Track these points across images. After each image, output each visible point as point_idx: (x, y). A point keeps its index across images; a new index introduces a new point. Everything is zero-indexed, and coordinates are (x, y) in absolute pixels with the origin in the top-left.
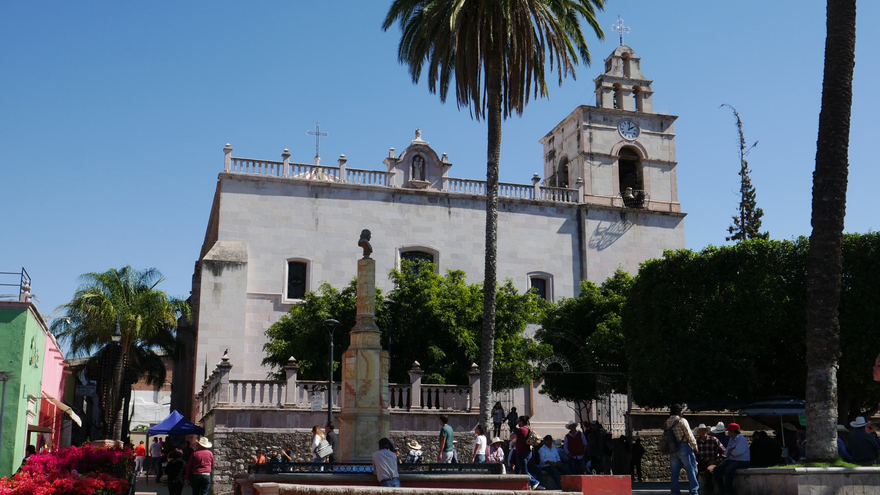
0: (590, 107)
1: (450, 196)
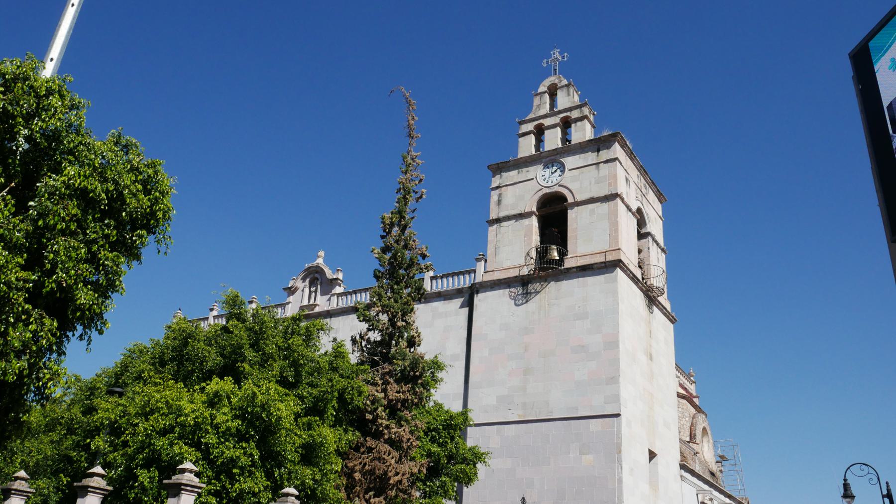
0: (498, 164)
1: (331, 312)
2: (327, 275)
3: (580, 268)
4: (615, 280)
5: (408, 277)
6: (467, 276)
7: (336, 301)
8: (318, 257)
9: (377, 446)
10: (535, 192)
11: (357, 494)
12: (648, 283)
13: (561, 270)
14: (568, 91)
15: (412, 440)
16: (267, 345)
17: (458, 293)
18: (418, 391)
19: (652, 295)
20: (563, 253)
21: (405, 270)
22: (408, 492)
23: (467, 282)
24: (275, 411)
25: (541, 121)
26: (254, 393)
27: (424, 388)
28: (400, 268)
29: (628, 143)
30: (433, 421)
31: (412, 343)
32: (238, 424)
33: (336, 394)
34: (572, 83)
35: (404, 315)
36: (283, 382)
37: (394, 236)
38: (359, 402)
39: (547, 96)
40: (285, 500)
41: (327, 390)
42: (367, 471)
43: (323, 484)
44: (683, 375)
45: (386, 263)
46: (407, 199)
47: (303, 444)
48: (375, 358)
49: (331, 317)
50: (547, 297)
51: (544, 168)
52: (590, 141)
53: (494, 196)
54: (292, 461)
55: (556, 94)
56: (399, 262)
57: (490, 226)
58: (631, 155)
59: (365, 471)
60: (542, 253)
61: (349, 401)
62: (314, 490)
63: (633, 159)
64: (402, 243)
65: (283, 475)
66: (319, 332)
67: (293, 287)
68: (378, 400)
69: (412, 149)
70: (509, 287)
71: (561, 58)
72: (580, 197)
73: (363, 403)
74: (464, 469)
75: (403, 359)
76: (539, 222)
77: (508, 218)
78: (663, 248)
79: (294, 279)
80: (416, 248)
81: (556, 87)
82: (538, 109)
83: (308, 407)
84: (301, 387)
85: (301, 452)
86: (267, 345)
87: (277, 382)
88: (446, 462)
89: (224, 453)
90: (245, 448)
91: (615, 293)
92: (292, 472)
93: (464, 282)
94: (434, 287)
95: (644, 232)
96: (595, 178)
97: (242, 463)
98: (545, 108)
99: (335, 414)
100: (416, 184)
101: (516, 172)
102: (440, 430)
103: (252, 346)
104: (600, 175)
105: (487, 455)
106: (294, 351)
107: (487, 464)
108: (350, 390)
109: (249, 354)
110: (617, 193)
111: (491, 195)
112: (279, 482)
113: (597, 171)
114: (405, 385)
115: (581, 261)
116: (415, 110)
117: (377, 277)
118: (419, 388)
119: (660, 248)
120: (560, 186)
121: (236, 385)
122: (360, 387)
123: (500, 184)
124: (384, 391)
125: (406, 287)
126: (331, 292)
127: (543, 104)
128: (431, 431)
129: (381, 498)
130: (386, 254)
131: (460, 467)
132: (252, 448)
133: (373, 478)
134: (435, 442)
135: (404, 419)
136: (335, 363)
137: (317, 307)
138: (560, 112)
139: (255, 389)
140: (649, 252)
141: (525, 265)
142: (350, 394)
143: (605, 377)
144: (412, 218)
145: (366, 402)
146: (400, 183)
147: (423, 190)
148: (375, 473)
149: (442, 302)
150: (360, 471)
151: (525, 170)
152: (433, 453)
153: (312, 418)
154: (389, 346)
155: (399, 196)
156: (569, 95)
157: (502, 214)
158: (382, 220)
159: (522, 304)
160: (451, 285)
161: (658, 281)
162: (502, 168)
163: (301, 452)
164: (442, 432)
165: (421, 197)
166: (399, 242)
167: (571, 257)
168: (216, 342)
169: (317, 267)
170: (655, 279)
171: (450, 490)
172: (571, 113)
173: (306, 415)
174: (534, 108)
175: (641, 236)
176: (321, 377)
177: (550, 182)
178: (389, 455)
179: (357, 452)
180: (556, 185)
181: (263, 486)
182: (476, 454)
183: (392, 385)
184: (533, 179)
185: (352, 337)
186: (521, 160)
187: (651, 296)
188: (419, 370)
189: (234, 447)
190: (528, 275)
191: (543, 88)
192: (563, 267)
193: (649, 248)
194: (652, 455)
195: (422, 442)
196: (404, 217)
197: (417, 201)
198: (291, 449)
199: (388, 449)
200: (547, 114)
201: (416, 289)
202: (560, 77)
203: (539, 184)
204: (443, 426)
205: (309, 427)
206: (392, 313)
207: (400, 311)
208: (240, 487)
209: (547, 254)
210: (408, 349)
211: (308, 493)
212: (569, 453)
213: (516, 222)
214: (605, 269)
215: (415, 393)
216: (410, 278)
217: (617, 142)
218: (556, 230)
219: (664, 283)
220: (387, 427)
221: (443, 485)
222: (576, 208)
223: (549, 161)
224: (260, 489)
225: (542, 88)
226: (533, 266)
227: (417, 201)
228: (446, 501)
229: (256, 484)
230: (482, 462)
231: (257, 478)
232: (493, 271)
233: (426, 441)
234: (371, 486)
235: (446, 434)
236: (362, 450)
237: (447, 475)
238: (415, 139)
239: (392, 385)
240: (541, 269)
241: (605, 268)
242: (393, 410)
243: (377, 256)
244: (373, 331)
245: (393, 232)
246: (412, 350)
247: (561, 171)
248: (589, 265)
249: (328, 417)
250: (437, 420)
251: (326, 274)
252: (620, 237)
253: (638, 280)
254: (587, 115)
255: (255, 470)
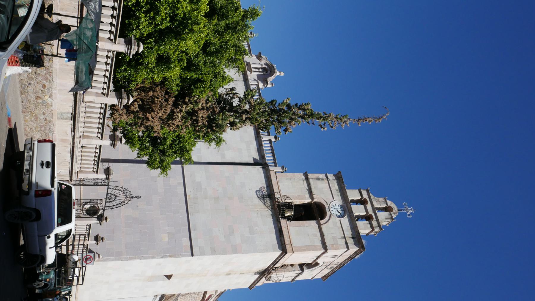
0: (342, 177)
2: (270, 78)
3: (280, 229)
4: (274, 251)
5: (273, 121)
6: (273, 161)
7: (254, 84)
8: (280, 72)
9: (169, 104)
10: (326, 200)
11: (140, 93)
12: (273, 271)
13: (279, 217)
14: (389, 218)
15: (173, 126)
16: (228, 34)
17: (262, 156)
18: (204, 129)
19: (266, 274)
20: (289, 218)
21: (277, 119)
22: (142, 125)
23: (269, 162)
24: (190, 37)
25: (369, 203)
26: (199, 24)
27: (205, 134)
28: (277, 116)
29: (358, 256)
30: (185, 140)
31: (233, 125)
32: (180, 15)
33: (200, 77)
34: (393, 221)
35: (250, 119)
36: (207, 45)
37: (297, 112)
38: (196, 92)
39: (385, 206)
40: (135, 45)
41: (203, 71)
42: (154, 99)
43: (145, 69)
44: (217, 297)
45: (280, 107)
46: (320, 119)
47: (169, 56)
48: (223, 102)
49: (244, 81)
50: (262, 209)
51: (340, 205)
52: (359, 233)
53: (322, 176)
54: (159, 50)
55: (386, 211)
56: (282, 115)
57: (303, 174)
58: (351, 258)
59: (154, 98)
60: (289, 206)
61: (196, 86)
62: (141, 64)
63: (348, 260)
64: (293, 117)
65: (151, 44)
66: (237, 68)
67: (261, 58)
68: (197, 105)
69: (351, 121)
70: (267, 187)
71: (408, 213)
72: (324, 227)
73: (195, 95)
74: (156, 161)
75: (222, 119)
76: (307, 203)
77: (309, 185)
78: (294, 280)
79: (266, 59)
80: (290, 125)
81: (391, 211)
82: (376, 200)
83: (192, 60)
84: (204, 56)
85: (165, 55)
86: (228, 34)
87: (206, 41)
88: (161, 149)
89: (163, 7)
90: (166, 20)
91: (266, 250)
92: (152, 50)
93: (269, 160)
94: (265, 142)
95: (304, 268)
96: (336, 236)
97: (157, 18)
98: (378, 205)
99: (188, 77)
100: (330, 124)
101: (337, 188)
102: (180, 145)
103: (227, 25)
104: (338, 239)
105: (166, 174)
106: (225, 52)
107: (160, 175)
108: (203, 86)
109: (223, 23)
110: (327, 250)
111: (322, 174)
112: (146, 42)
113: (340, 237)
114: (207, 121)
115: (285, 229)
116: (375, 122)
117: (272, 102)
118: (205, 130)
119: (295, 278)
120: (330, 215)
121: (204, 14)
122: (205, 92)
123: (330, 179)
124: (203, 109)
125: (266, 120)
126: (259, 81)
127: (380, 203)
128: (179, 139)
129: (138, 109)
130: (286, 107)
131: (158, 158)
132: (166, 24)
133: (150, 103)
134: (172, 142)
135: (186, 121)
136: (219, 77)
137: (250, 73)
138: (375, 214)
139: (202, 25)
140: (292, 271)
141: (281, 196)
142: (201, 86)
143: (215, 246)
144: (308, 123)
145: (196, 97)
146: (330, 114)
147: (326, 129)
148: (153, 104)
149: (256, 147)
150: (153, 95)
151: (339, 194)
152: (166, 141)
153: (186, 61)
154: (230, 111)
155: (322, 114)
156: (386, 219)
157: (311, 181)
158: (307, 103)
159: (257, 195)
160: (267, 152)
161: (275, 277)
162: (339, 180)
163: (165, 55)
164: (178, 146)
165: (322, 127)
166: (294, 115)
167: (287, 223)
168: (230, 3)
169: (274, 72)
170: (276, 275)
171: (144, 152)
172: (375, 220)
173: (187, 59)
174: (377, 198)
175: (301, 266)
176: (210, 68)
177: (332, 209)
178: (164, 112)
179: (165, 93)
180: (331, 213)
181: (144, 32)
182: (166, 168)
183: (206, 113)
184: (333, 199)
185: (235, 88)
186: (345, 191)
187: (264, 273)
188: (216, 129)
189: (167, 13)
190: (275, 197)
191: (390, 204)
192: (280, 218)
193: (294, 271)
194: (169, 277)
195: (172, 134)
196: (309, 118)
197: (319, 125)
198: (166, 49)
199: (168, 111)
200: (374, 206)
201: (266, 126)
202: (397, 213)
203: (331, 203)
204: (183, 146)
205: (180, 60)
206: (250, 112)
207: (252, 116)
208: (142, 17)
209: (289, 208)
210: (229, 122)
211: (140, 60)
212: (168, 227)
213: (307, 189)
214: (280, 244)
215: (202, 128)
216: (271, 122)
217: (358, 249)
218: (303, 214)
219: (274, 281)
220: (181, 111)
221: (146, 148)
222: (317, 225)
223: (345, 208)
224: (141, 30)
225: (389, 203)
226: (280, 201)
227: (319, 125)
228: (137, 151)
229: (145, 27)
230: (161, 172)
231: (148, 28)
232: (276, 177)
233: (173, 136)
234: (145, 102)
235: (178, 149)
236: (167, 96)
237: (153, 150)
238: (357, 123)
239: (206, 113)
240: (279, 206)
241: (281, 244)
242: (192, 114)
243: (285, 101)
244: (239, 100)
245: (300, 111)
246: (228, 125)
247: (339, 215)
248: (283, 234)
249: (186, 73)
250: (186, 143)
251: (270, 77)
252: (300, 252)
253: (275, 265)
254: (374, 230)
255: (153, 26)
